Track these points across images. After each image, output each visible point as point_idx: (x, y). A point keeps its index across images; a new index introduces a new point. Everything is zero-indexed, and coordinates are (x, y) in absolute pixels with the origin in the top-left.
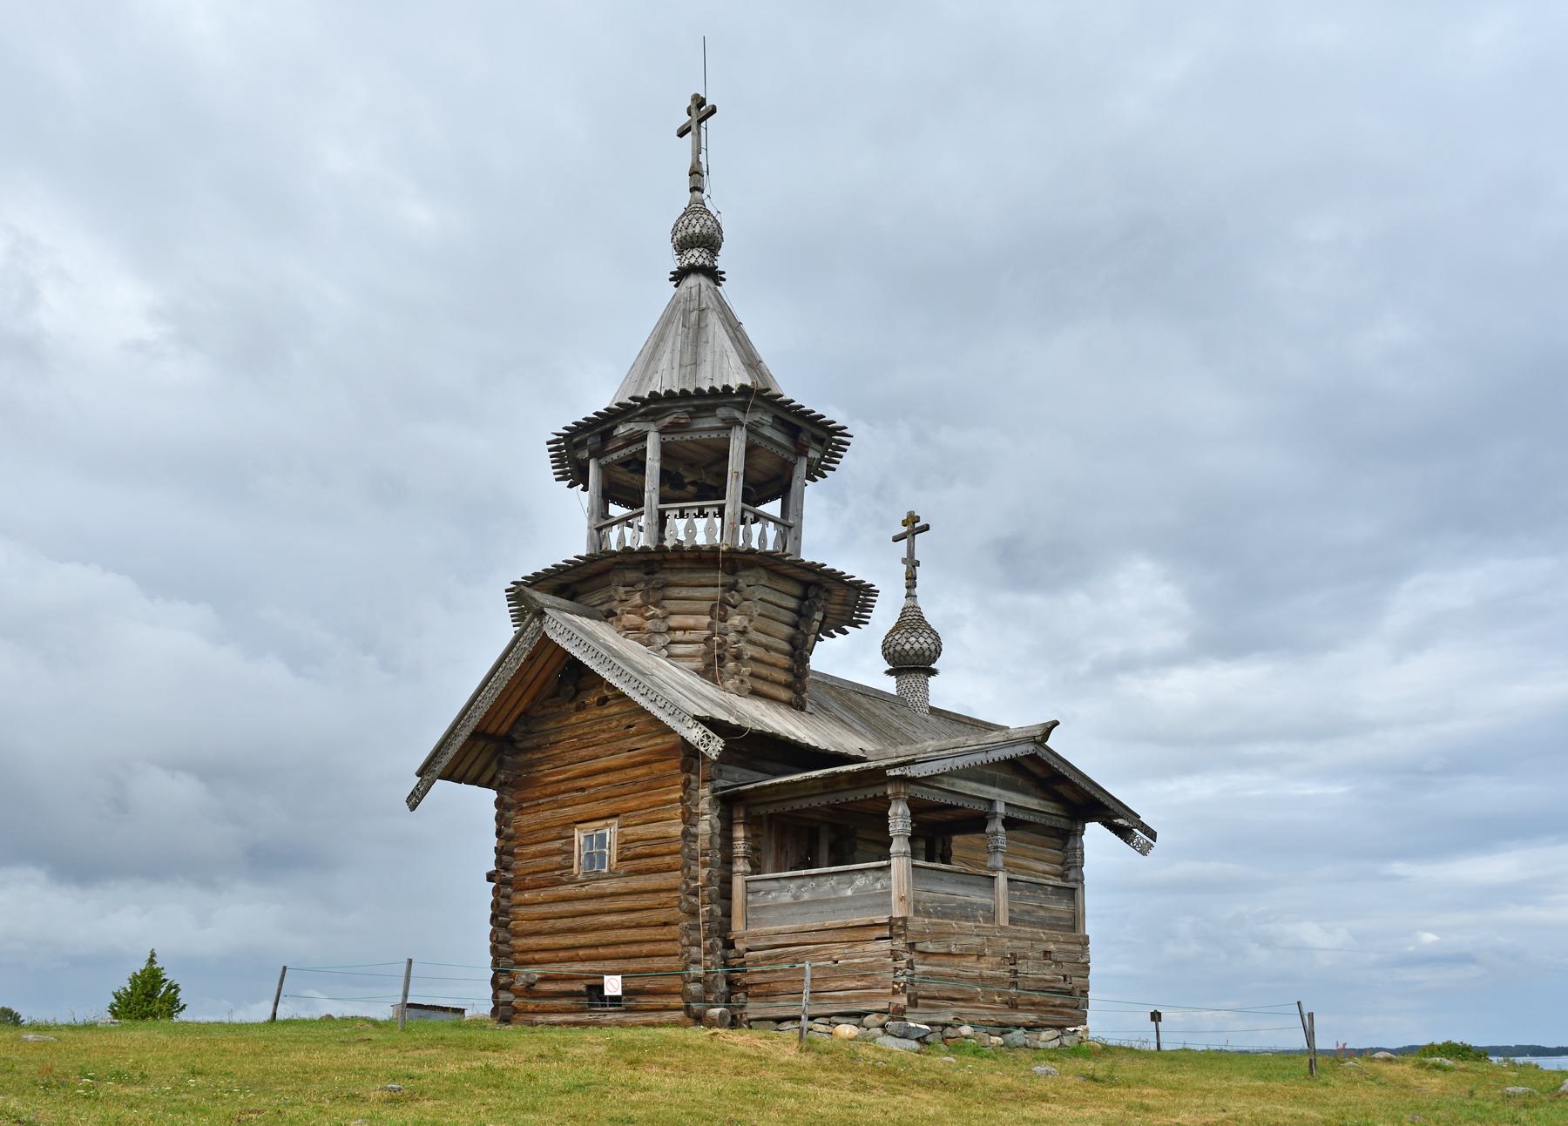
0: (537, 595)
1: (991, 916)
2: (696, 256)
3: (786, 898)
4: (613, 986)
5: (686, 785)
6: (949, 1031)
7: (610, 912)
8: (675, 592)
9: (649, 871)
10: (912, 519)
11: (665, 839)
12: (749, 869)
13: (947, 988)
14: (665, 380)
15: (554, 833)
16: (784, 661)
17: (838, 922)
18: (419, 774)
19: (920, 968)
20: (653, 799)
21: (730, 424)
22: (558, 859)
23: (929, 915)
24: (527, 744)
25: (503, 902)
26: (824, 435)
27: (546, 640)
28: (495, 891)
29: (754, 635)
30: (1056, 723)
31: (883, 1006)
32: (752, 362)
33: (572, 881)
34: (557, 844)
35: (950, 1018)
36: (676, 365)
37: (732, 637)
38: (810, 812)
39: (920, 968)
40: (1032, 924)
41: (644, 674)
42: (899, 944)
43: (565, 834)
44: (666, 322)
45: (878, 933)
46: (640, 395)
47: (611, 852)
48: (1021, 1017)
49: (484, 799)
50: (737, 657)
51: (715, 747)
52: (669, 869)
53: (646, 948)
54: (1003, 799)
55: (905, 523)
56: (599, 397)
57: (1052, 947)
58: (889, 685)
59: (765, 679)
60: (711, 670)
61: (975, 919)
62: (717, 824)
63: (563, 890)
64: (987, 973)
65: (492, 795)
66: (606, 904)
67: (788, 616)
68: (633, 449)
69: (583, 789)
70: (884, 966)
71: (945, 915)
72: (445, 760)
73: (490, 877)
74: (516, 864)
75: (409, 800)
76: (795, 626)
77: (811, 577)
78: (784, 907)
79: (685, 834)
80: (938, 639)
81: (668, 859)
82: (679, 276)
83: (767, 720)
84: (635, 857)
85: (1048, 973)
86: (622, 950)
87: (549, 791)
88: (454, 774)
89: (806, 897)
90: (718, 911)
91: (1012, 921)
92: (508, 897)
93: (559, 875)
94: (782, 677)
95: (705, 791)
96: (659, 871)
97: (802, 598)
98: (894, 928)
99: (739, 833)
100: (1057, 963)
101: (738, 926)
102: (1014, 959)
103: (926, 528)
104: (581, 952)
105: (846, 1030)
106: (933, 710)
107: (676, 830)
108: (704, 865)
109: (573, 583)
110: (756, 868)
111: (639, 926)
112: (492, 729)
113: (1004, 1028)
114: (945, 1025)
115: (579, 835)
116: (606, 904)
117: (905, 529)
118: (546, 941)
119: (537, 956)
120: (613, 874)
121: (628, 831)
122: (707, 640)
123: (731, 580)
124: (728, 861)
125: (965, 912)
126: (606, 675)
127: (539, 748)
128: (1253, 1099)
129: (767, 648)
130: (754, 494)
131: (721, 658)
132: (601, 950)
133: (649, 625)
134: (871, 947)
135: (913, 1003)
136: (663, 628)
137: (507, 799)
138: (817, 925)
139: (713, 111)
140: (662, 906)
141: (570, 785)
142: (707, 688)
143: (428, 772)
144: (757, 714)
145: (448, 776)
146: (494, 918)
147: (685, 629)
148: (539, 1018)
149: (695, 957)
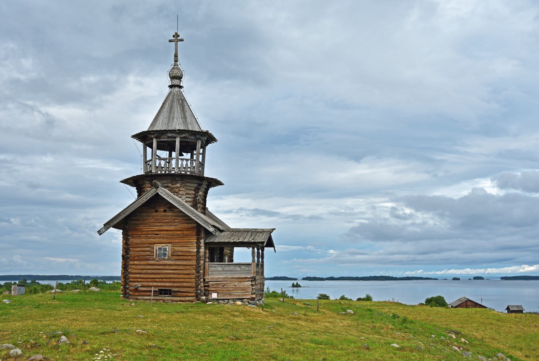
2: (176, 82)
3: (220, 269)
14: (159, 127)
20: (184, 241)
22: (149, 253)
31: (249, 297)
34: (148, 249)
42: (254, 283)
45: (248, 280)
53: (181, 280)
63: (150, 262)
65: (122, 231)
66: (167, 267)
68: (172, 139)
69: (157, 234)
70: (249, 288)
82: (171, 87)
86: (172, 280)
87: (144, 233)
105: (239, 303)
107: (196, 250)
116: (167, 267)
119: (139, 280)
120: (169, 259)
134: (246, 283)
138: (230, 277)
143: (107, 225)
148: (140, 297)
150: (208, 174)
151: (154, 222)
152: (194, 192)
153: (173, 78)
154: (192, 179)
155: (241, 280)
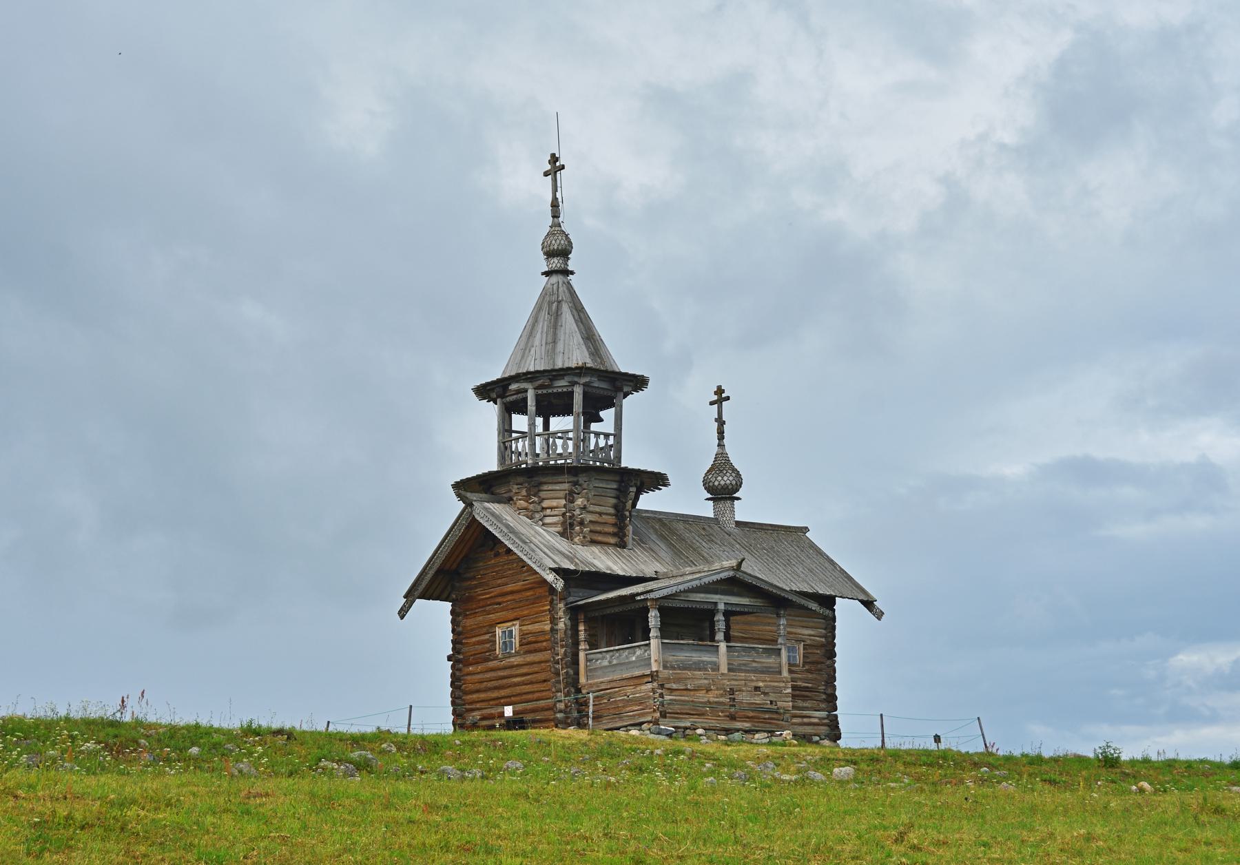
1: (716, 667)
2: (556, 263)
3: (606, 663)
4: (508, 711)
5: (551, 602)
6: (688, 732)
7: (517, 676)
8: (545, 487)
9: (536, 651)
11: (543, 632)
13: (686, 709)
14: (533, 364)
15: (485, 630)
16: (612, 520)
17: (628, 675)
19: (667, 698)
21: (573, 384)
23: (673, 668)
24: (468, 575)
25: (458, 673)
28: (453, 667)
29: (592, 508)
31: (649, 718)
32: (590, 338)
33: (496, 658)
34: (487, 637)
35: (688, 724)
37: (577, 512)
39: (667, 698)
40: (746, 671)
41: (525, 543)
42: (655, 684)
44: (539, 308)
47: (516, 641)
48: (738, 725)
49: (443, 609)
50: (581, 523)
51: (559, 585)
52: (546, 650)
54: (722, 601)
55: (716, 393)
56: (496, 375)
57: (761, 684)
58: (706, 509)
59: (600, 533)
60: (566, 532)
61: (706, 670)
62: (569, 623)
63: (491, 664)
64: (712, 700)
65: (448, 606)
67: (613, 493)
70: (649, 697)
71: (685, 668)
73: (449, 658)
74: (465, 649)
75: (399, 613)
76: (617, 498)
78: (604, 666)
79: (552, 630)
80: (738, 474)
83: (596, 562)
84: (528, 644)
85: (758, 699)
87: (481, 604)
88: (426, 595)
90: (571, 672)
91: (729, 670)
92: (460, 670)
93: (487, 655)
94: (611, 529)
95: (561, 605)
97: (621, 482)
98: (653, 676)
99: (582, 628)
100: (765, 694)
101: (582, 680)
102: (732, 691)
103: (728, 398)
105: (634, 732)
106: (738, 524)
107: (548, 628)
108: (562, 646)
110: (593, 645)
111: (532, 683)
113: (728, 731)
114: (686, 728)
115: (498, 631)
117: (715, 398)
118: (482, 696)
119: (478, 706)
121: (524, 628)
122: (564, 515)
123: (575, 479)
124: (576, 643)
125: (699, 666)
126: (506, 543)
127: (474, 578)
128: (832, 756)
129: (600, 514)
131: (571, 525)
133: (531, 507)
134: (643, 687)
135: (664, 715)
136: (539, 508)
137: (458, 610)
138: (619, 677)
139: (563, 167)
140: (543, 670)
142: (562, 544)
143: (411, 596)
144: (590, 558)
145: (422, 597)
146: (452, 684)
147: (551, 508)
150: (629, 460)
151: (494, 578)
152: (564, 502)
153: (550, 254)
154: (554, 475)
155: (636, 681)
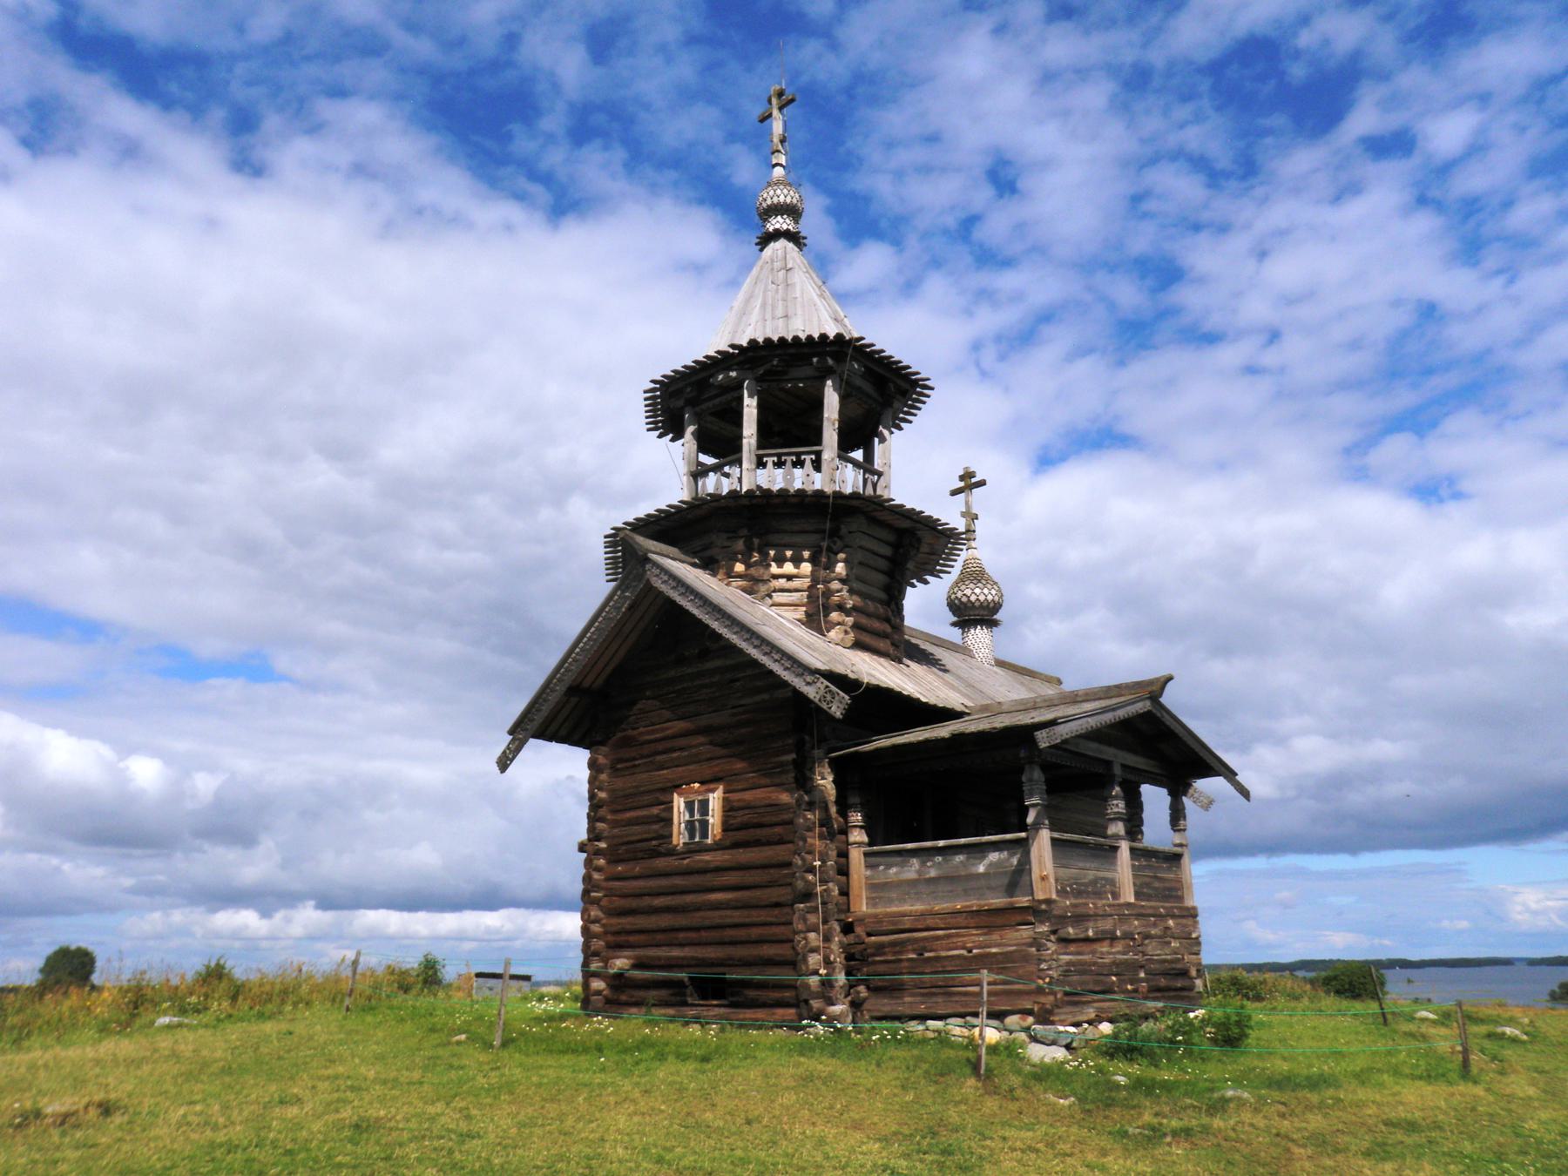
0: (640, 539)
9: (758, 843)
10: (967, 476)
12: (866, 839)
18: (511, 732)
26: (906, 386)
27: (649, 588)
28: (588, 863)
30: (1170, 678)
34: (655, 811)
36: (768, 316)
38: (952, 784)
43: (662, 798)
46: (737, 342)
47: (715, 819)
53: (755, 932)
55: (962, 478)
66: (710, 880)
72: (539, 718)
77: (906, 524)
81: (777, 830)
83: (877, 675)
89: (933, 873)
91: (1138, 895)
96: (769, 843)
97: (896, 546)
103: (982, 483)
104: (681, 935)
109: (687, 527)
112: (586, 684)
115: (679, 802)
116: (710, 880)
117: (962, 484)
119: (632, 939)
130: (845, 446)
132: (703, 934)
137: (601, 760)
141: (668, 744)
149: (814, 944)
